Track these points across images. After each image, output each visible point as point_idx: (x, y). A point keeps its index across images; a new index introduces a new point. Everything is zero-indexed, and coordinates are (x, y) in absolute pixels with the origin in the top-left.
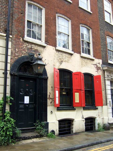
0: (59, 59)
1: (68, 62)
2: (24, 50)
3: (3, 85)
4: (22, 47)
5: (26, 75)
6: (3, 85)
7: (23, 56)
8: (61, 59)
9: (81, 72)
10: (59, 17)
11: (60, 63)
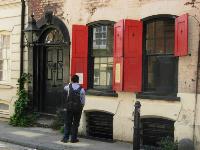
0: (89, 5)
1: (106, 6)
2: (41, 11)
3: (18, 34)
4: (39, 7)
5: (42, 57)
6: (18, 34)
7: (40, 19)
8: (92, 5)
9: (79, 77)
10: (51, 70)
11: (91, 13)
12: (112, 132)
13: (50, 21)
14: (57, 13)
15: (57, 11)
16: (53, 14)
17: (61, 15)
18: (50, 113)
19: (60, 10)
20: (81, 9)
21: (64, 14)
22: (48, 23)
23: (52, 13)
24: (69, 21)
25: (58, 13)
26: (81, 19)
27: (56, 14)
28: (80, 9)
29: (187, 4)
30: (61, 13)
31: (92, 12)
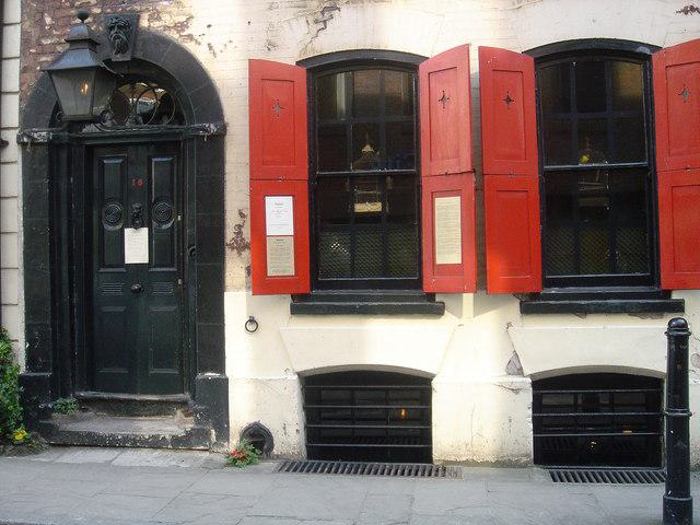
11: (316, 22)
12: (426, 437)
13: (131, 49)
14: (159, 19)
15: (159, 12)
16: (144, 23)
17: (181, 27)
18: (124, 392)
19: (174, 9)
20: (270, 9)
21: (193, 23)
22: (118, 56)
23: (138, 18)
24: (217, 48)
25: (167, 20)
26: (273, 40)
27: (156, 24)
28: (268, 6)
29: (685, 11)
30: (183, 19)
31: (320, 18)
